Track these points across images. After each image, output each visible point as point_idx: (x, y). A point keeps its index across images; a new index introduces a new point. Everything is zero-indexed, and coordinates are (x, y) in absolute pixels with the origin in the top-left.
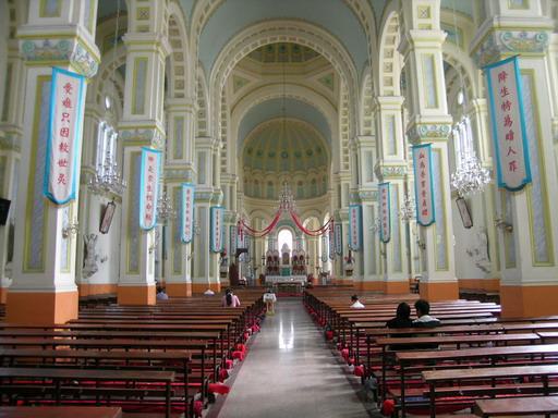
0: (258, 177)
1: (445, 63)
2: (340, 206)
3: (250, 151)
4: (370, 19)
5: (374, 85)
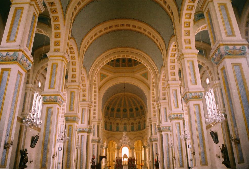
0: (112, 121)
1: (199, 65)
2: (152, 135)
3: (108, 108)
4: (163, 46)
5: (166, 76)
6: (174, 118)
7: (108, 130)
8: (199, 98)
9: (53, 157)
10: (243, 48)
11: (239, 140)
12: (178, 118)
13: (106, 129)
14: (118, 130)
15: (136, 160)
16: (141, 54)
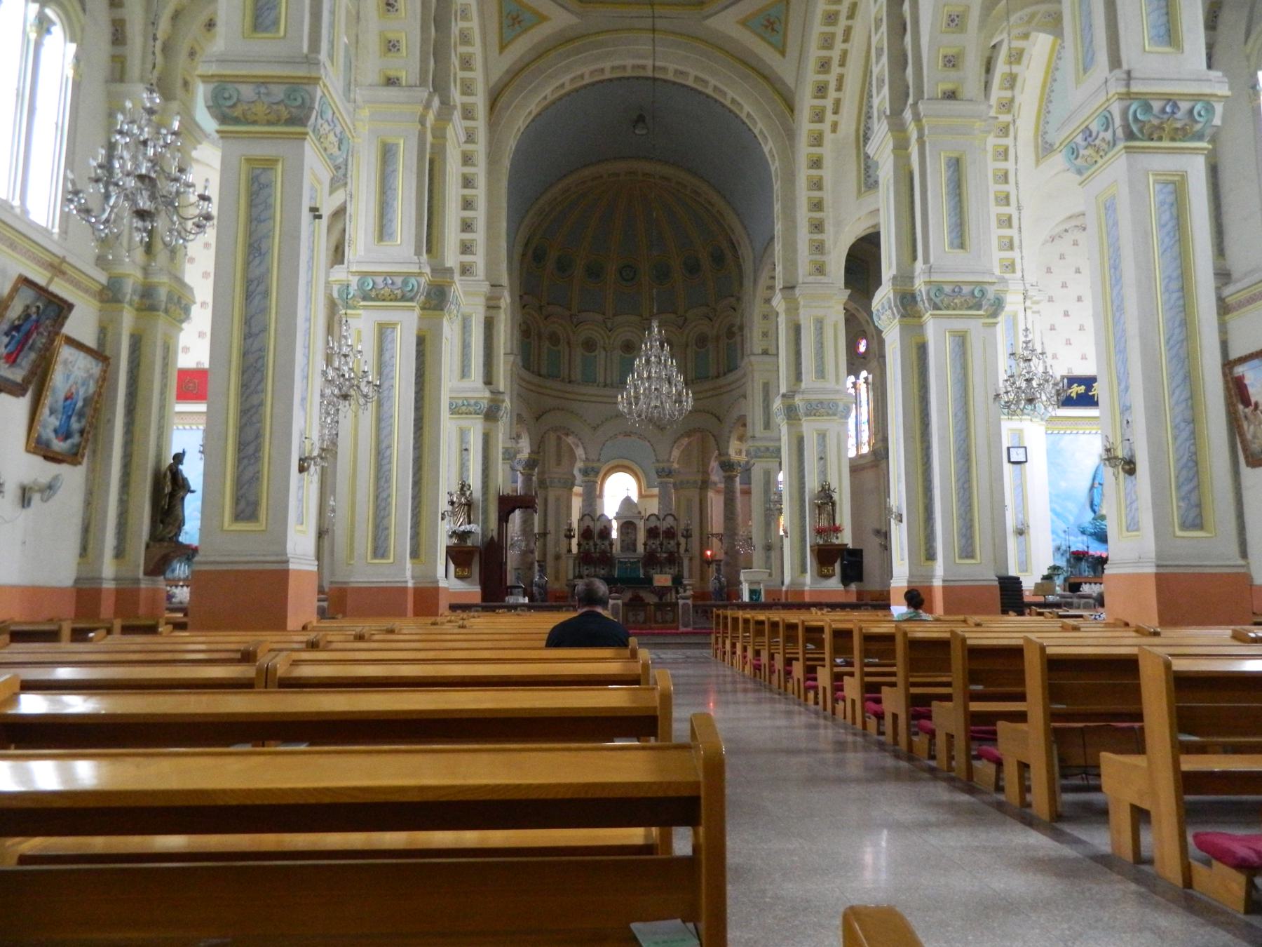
2: (798, 377)
7: (540, 375)
11: (1134, 464)
14: (589, 380)
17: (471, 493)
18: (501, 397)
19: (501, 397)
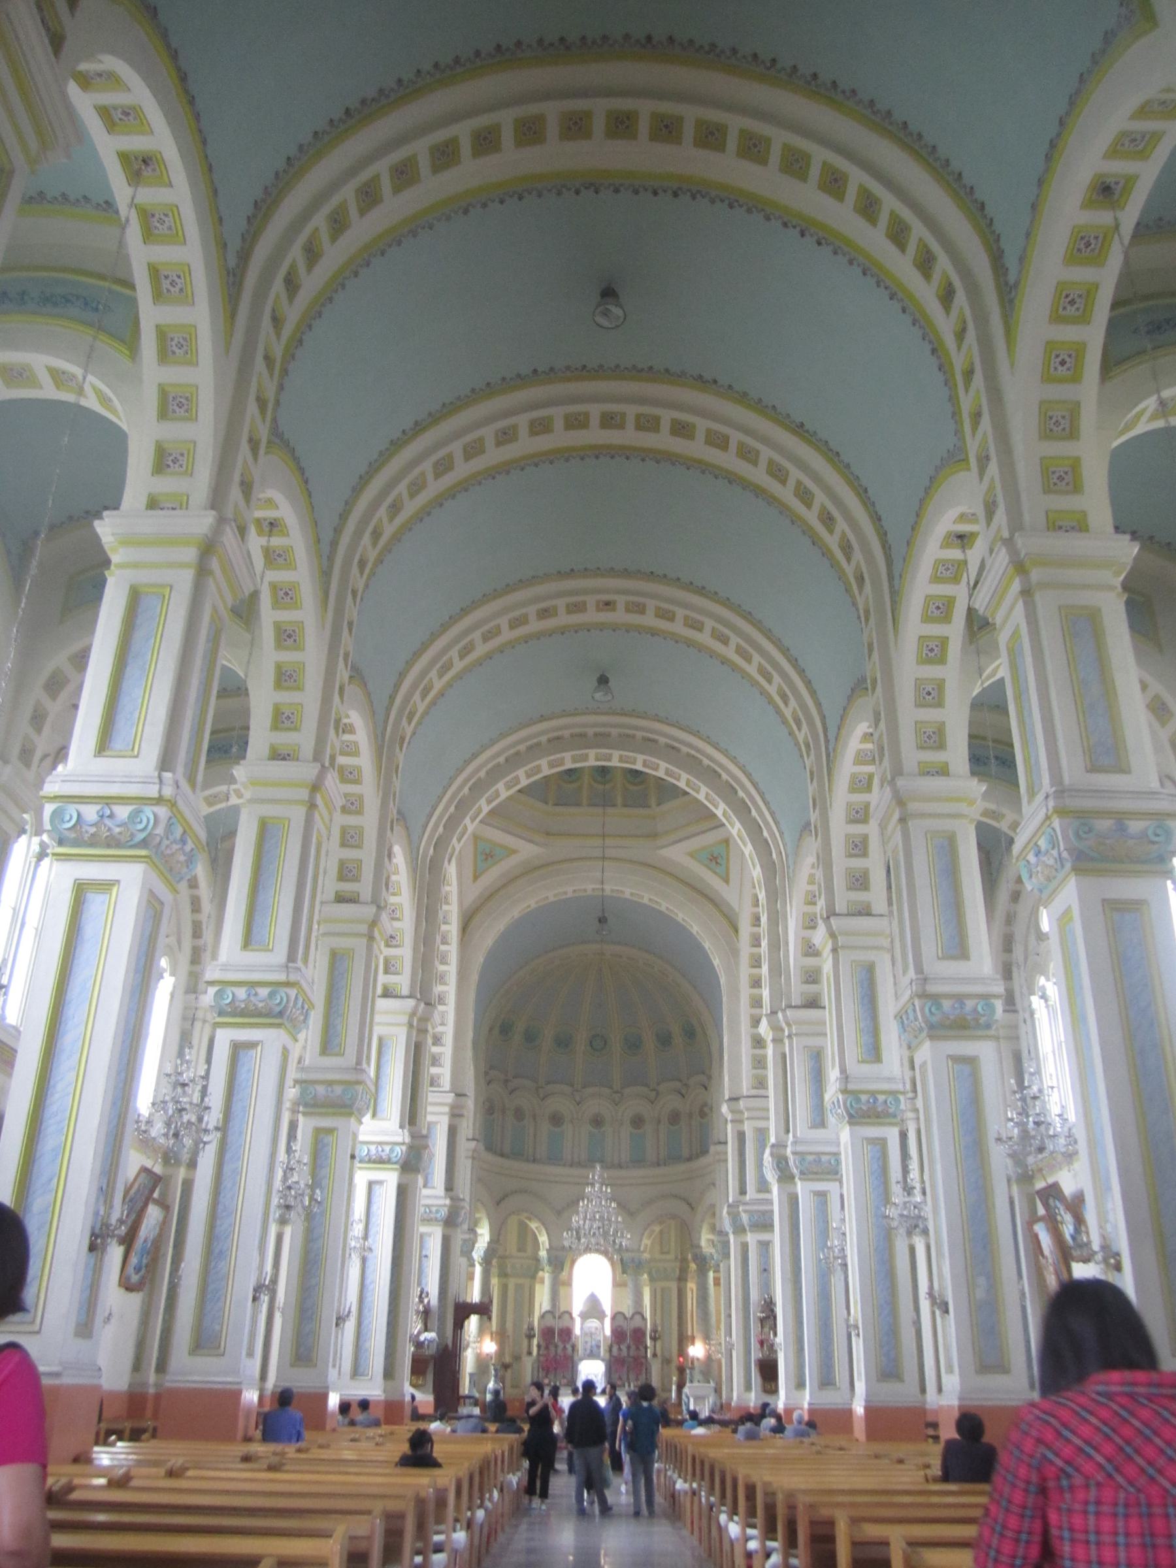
2: (743, 1192)
3: (505, 1029)
6: (857, 1113)
7: (502, 1155)
8: (978, 1026)
9: (337, 1325)
10: (1158, 832)
12: (878, 1117)
13: (489, 1148)
14: (554, 1158)
15: (654, 1331)
16: (698, 750)
17: (429, 1302)
18: (462, 1204)
19: (462, 1204)
